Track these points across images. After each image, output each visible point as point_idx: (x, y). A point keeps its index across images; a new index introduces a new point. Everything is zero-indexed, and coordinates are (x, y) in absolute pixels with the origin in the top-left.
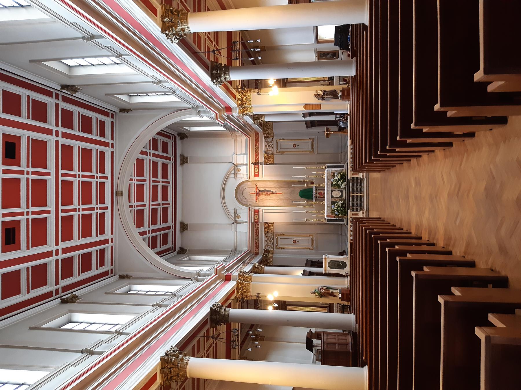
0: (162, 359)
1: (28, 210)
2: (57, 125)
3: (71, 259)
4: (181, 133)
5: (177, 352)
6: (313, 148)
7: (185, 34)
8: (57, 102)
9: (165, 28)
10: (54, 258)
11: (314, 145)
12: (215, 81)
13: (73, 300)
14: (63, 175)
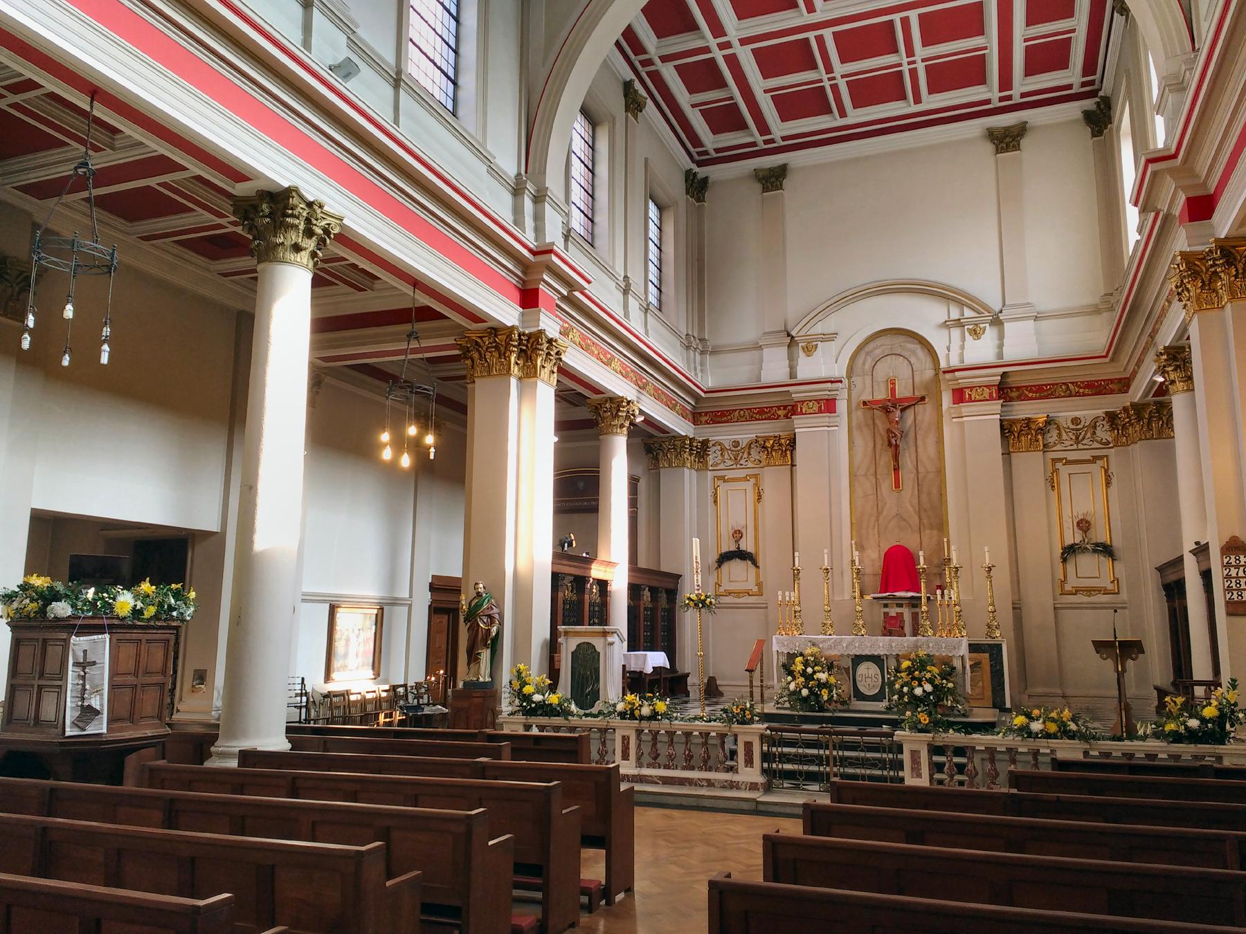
0: (288, 192)
10: (713, 42)
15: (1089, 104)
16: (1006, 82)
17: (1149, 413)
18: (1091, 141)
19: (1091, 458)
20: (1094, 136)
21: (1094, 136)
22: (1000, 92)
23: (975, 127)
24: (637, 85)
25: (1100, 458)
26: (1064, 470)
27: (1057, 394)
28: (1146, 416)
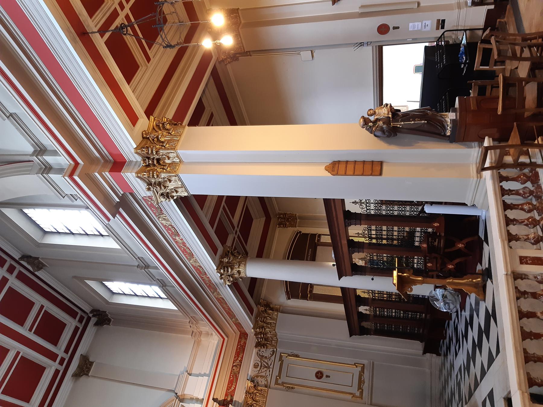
4: (99, 310)
6: (360, 389)
9: (220, 266)
11: (365, 381)
15: (94, 320)
16: (52, 356)
17: (261, 322)
18: (111, 326)
19: (280, 362)
20: (109, 324)
21: (109, 324)
22: (55, 361)
23: (68, 382)
25: (281, 357)
26: (283, 379)
27: (237, 373)
28: (263, 324)
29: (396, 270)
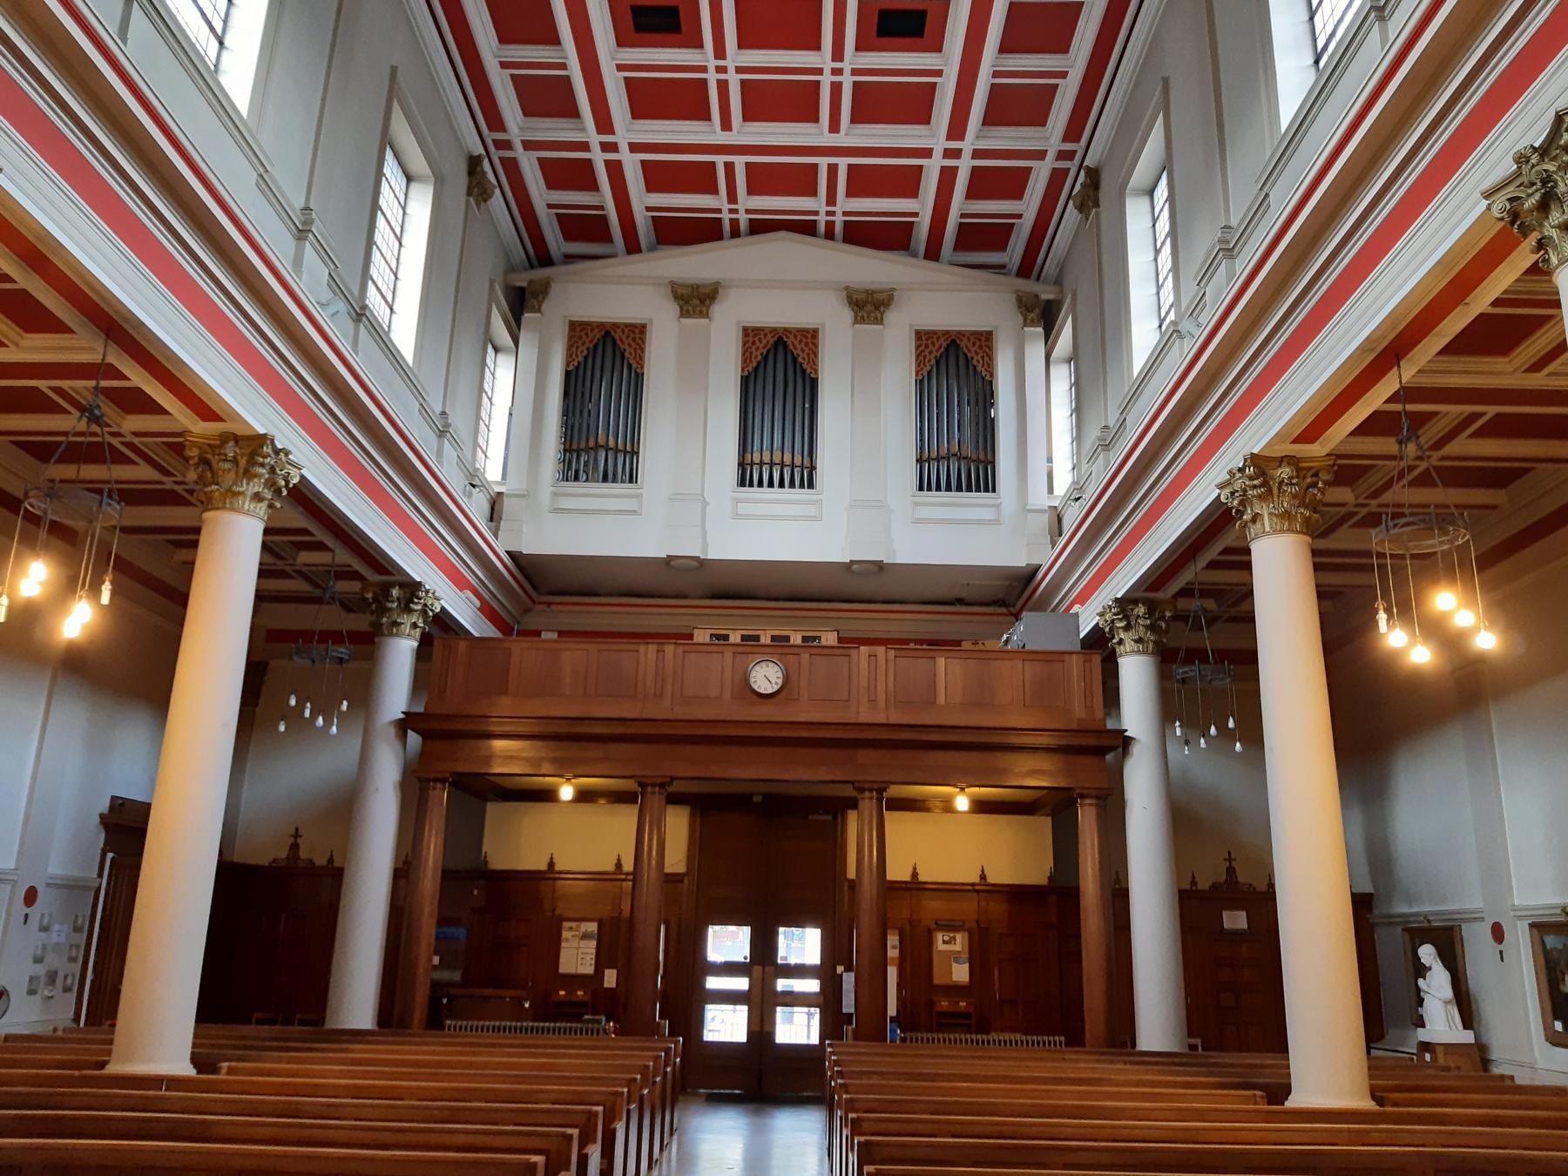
0: (262, 439)
1: (732, 70)
2: (977, 154)
3: (593, 186)
5: (283, 483)
7: (1245, 525)
8: (1050, 156)
9: (1259, 464)
10: (594, 139)
12: (1113, 610)
13: (477, 188)
14: (833, 169)
24: (486, 164)
29: (890, 1017)
